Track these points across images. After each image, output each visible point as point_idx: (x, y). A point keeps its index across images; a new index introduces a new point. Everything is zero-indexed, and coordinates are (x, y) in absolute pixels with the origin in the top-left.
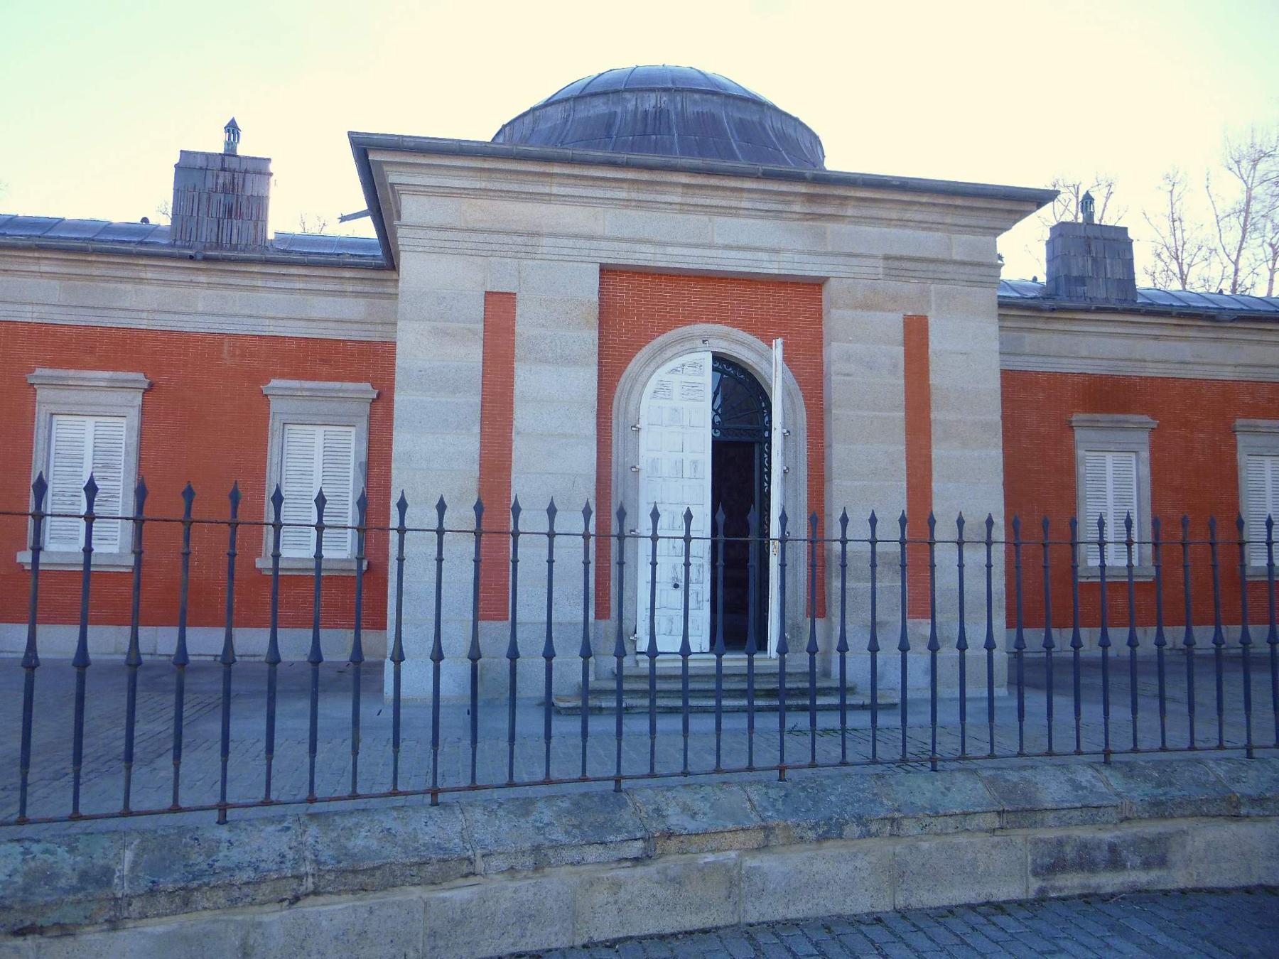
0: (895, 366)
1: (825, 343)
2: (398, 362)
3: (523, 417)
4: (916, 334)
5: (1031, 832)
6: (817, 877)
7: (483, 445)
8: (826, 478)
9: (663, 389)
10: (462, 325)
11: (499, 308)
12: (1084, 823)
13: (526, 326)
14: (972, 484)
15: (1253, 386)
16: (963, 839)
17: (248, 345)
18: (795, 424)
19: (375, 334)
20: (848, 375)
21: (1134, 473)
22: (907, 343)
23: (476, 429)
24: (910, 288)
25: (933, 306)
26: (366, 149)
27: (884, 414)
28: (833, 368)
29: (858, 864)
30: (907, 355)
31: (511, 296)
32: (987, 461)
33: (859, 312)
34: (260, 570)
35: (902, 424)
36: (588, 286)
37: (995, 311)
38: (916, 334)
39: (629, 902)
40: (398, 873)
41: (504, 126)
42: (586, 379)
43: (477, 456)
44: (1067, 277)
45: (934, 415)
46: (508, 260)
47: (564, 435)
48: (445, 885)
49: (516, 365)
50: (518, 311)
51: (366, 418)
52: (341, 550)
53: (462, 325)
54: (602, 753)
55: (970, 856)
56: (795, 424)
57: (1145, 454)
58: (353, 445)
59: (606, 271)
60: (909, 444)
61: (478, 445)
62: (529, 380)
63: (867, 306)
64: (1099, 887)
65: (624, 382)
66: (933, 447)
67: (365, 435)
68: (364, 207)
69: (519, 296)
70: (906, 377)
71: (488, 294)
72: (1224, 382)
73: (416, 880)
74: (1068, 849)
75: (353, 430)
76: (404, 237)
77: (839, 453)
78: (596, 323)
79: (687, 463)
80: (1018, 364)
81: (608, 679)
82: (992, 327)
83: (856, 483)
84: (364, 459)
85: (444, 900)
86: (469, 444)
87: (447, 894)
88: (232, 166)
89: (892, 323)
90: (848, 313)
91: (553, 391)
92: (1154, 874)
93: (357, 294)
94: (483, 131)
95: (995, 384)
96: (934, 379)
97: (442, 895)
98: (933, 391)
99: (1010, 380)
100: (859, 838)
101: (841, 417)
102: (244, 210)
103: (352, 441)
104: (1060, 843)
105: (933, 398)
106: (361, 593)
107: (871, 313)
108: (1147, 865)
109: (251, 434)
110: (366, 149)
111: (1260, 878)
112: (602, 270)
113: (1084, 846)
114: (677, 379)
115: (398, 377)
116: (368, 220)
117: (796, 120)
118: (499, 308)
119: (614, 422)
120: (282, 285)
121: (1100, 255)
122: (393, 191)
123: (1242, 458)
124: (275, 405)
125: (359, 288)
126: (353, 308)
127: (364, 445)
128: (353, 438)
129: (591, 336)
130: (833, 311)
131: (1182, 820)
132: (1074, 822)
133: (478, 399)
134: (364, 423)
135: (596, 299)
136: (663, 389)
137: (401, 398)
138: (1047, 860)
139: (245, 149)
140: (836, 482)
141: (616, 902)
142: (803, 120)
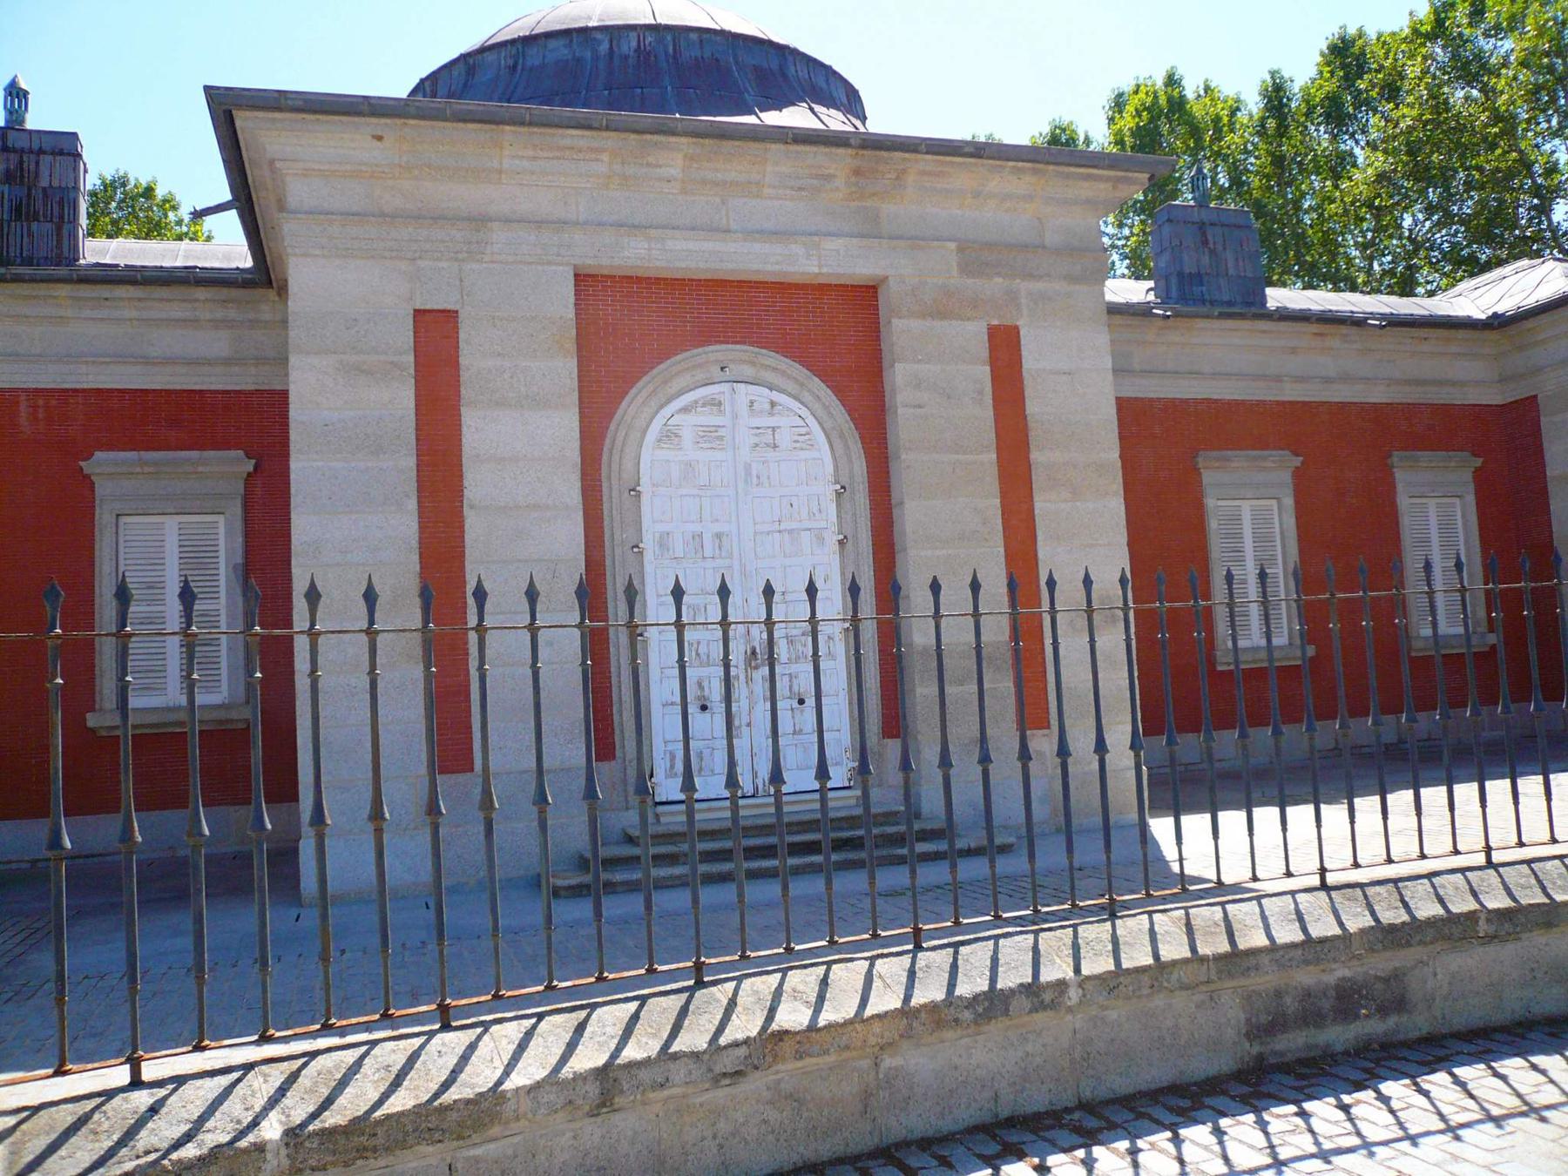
0: (981, 392)
1: (886, 364)
2: (292, 413)
3: (478, 484)
4: (1004, 349)
5: (1243, 982)
6: (978, 1072)
7: (422, 528)
8: (897, 548)
9: (670, 436)
10: (382, 358)
11: (436, 336)
12: (1307, 962)
13: (476, 356)
14: (1088, 540)
15: (1409, 411)
16: (1159, 1001)
17: (57, 403)
18: (852, 477)
19: (243, 380)
20: (920, 407)
21: (1277, 525)
22: (994, 362)
23: (412, 504)
24: (995, 286)
25: (1025, 312)
26: (226, 108)
27: (970, 457)
28: (899, 399)
29: (1029, 1048)
30: (995, 378)
31: (449, 318)
32: (1106, 513)
33: (928, 323)
34: (93, 730)
35: (994, 471)
36: (561, 301)
37: (1105, 317)
38: (1004, 349)
39: (733, 1135)
40: (410, 1128)
41: (422, 81)
42: (564, 426)
43: (415, 543)
44: (1180, 275)
45: (1036, 456)
46: (445, 264)
47: (537, 507)
48: (476, 1138)
49: (463, 410)
50: (462, 336)
51: (238, 503)
52: (222, 689)
53: (382, 358)
54: (631, 944)
55: (1169, 1023)
56: (852, 477)
57: (1289, 502)
58: (222, 542)
59: (583, 280)
60: (1004, 495)
61: (415, 526)
62: (482, 432)
63: (941, 314)
64: (1328, 1046)
65: (617, 431)
66: (1036, 498)
67: (239, 525)
68: (227, 196)
69: (461, 316)
70: (995, 407)
71: (417, 313)
72: (1375, 407)
73: (437, 1136)
74: (1288, 1000)
75: (221, 519)
76: (291, 235)
77: (913, 515)
78: (571, 346)
79: (707, 538)
80: (1129, 392)
81: (618, 843)
82: (1103, 339)
83: (938, 552)
84: (239, 559)
85: (477, 1160)
86: (404, 524)
87: (478, 1151)
88: (18, 145)
89: (972, 334)
90: (916, 325)
91: (518, 445)
92: (1392, 1021)
93: (217, 324)
94: (399, 87)
95: (1111, 412)
96: (1032, 407)
97: (478, 1151)
98: (1031, 424)
99: (1123, 405)
100: (1031, 1012)
101: (913, 465)
102: (39, 204)
103: (224, 535)
104: (1278, 994)
105: (1032, 434)
106: (252, 753)
107: (945, 323)
108: (1383, 1011)
109: (70, 524)
110: (226, 108)
111: (1513, 1011)
112: (576, 275)
113: (1307, 994)
114: (691, 419)
115: (293, 436)
116: (232, 216)
117: (829, 68)
118: (436, 336)
119: (605, 485)
120: (104, 313)
121: (1220, 248)
122: (273, 170)
123: (1403, 502)
124: (103, 488)
125: (219, 314)
126: (217, 344)
127: (239, 540)
128: (222, 530)
129: (567, 368)
130: (895, 321)
131: (1420, 948)
132: (1294, 963)
133: (411, 462)
134: (237, 509)
135: (570, 313)
136: (670, 436)
137: (301, 467)
138: (1264, 1019)
139: (37, 119)
140: (912, 552)
141: (715, 1137)
142: (835, 68)
